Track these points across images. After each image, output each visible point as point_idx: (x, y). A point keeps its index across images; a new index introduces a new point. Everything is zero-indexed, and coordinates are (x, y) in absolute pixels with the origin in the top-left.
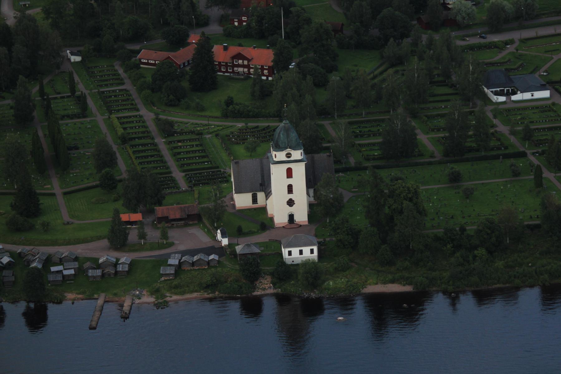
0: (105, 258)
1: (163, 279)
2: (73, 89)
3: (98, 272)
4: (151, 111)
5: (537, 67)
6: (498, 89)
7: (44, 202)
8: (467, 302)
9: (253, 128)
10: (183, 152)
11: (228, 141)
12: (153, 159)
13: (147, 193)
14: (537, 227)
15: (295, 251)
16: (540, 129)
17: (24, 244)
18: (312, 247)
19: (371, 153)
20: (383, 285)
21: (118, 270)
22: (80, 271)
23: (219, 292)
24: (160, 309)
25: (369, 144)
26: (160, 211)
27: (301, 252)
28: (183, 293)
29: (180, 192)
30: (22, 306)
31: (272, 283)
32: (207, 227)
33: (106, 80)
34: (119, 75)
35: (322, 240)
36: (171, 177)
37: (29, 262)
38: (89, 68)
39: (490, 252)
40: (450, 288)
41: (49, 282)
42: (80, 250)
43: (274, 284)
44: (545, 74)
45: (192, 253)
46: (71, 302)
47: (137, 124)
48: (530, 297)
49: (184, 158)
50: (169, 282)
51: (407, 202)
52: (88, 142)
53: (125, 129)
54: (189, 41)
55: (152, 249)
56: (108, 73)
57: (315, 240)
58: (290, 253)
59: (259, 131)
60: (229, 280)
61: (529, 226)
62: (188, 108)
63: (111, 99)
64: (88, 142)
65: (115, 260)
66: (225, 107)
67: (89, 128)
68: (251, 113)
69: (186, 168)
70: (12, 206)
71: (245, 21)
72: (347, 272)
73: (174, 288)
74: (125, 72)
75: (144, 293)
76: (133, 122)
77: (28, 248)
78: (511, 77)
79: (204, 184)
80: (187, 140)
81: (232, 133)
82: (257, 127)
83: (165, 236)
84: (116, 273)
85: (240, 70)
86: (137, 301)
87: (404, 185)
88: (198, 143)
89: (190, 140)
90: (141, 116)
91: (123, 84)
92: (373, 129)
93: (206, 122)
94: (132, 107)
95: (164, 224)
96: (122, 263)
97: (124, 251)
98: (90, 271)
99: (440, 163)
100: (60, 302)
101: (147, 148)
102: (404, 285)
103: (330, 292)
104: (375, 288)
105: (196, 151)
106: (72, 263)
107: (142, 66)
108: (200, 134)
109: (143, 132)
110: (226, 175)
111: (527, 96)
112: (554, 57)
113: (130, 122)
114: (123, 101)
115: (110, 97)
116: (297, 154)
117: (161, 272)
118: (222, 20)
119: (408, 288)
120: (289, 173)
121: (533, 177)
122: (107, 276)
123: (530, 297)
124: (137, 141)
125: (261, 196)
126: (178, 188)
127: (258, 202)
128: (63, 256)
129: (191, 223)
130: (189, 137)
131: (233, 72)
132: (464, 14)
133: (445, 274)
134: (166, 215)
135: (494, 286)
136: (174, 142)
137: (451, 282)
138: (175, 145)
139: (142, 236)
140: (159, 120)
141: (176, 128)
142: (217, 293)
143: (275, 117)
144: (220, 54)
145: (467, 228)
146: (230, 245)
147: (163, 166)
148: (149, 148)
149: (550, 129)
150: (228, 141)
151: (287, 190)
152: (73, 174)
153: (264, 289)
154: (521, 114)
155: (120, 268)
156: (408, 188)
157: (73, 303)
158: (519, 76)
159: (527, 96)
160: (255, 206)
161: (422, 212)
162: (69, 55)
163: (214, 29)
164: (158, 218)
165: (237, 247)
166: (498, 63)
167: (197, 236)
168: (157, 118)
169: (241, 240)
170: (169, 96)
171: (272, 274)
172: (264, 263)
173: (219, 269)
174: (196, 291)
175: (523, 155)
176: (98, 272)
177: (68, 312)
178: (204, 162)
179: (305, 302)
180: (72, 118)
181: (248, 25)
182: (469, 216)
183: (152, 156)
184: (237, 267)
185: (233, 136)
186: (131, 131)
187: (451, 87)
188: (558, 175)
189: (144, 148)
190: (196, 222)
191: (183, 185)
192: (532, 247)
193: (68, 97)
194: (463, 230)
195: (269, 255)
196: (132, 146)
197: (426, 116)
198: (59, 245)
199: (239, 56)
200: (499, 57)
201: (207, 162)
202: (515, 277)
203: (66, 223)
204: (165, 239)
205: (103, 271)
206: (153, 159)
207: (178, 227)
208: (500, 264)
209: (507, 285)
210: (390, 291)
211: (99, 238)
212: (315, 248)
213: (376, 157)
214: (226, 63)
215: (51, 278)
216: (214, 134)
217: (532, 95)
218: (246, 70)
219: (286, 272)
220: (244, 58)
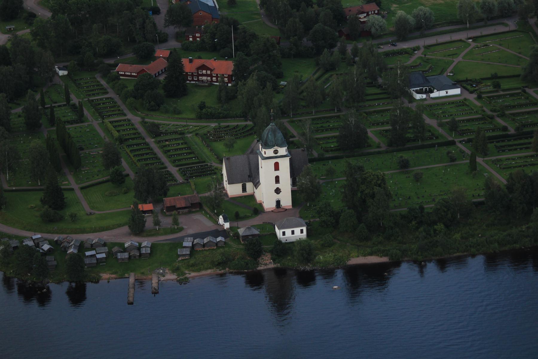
0: (130, 243)
1: (180, 259)
2: (68, 99)
3: (126, 255)
4: (136, 115)
5: (443, 69)
6: (418, 88)
7: (67, 195)
8: (431, 268)
9: (225, 128)
10: (172, 150)
11: (208, 139)
12: (148, 156)
13: (154, 187)
14: (481, 203)
15: (288, 232)
16: (460, 121)
17: (57, 233)
18: (302, 228)
19: (328, 145)
20: (364, 258)
21: (142, 252)
22: (110, 254)
23: (230, 268)
24: (183, 284)
25: (324, 138)
26: (168, 201)
27: (293, 232)
28: (199, 270)
29: (178, 184)
30: (66, 285)
31: (272, 259)
32: (208, 214)
33: (93, 90)
34: (102, 85)
35: (307, 221)
36: (168, 171)
37: (66, 249)
38: (75, 80)
39: (447, 226)
40: (420, 258)
41: (86, 265)
42: (106, 236)
43: (274, 260)
44: (451, 74)
45: (202, 235)
46: (107, 281)
47: (127, 127)
48: (477, 263)
49: (174, 155)
50: (186, 261)
51: (377, 188)
52: (90, 144)
53: (118, 131)
54: (156, 55)
55: (166, 233)
56: (92, 84)
57: (301, 220)
58: (284, 233)
59: (230, 130)
60: (236, 258)
61: (474, 203)
62: (167, 112)
63: (100, 106)
64: (90, 144)
65: (138, 244)
66: (199, 110)
67: (88, 131)
68: (221, 115)
69: (177, 163)
70: (41, 201)
71: (198, 37)
72: (332, 248)
73: (191, 266)
74: (108, 83)
75: (167, 271)
76: (124, 125)
77: (64, 236)
78: (427, 78)
79: (196, 176)
80: (173, 139)
81: (209, 132)
82: (228, 126)
83: (176, 222)
84: (141, 255)
85: (204, 78)
86: (162, 279)
87: (373, 173)
88: (182, 142)
89: (175, 139)
90: (129, 120)
91: (107, 93)
92: (324, 125)
93: (185, 124)
94: (119, 112)
95: (174, 212)
96: (145, 247)
97: (143, 236)
98: (119, 254)
99: (387, 152)
100: (97, 282)
101: (140, 147)
102: (381, 257)
103: (321, 265)
104: (357, 260)
105: (182, 149)
106: (103, 248)
107: (121, 77)
108: (182, 133)
109: (135, 134)
110: (213, 168)
111: (443, 93)
112: (454, 60)
113: (121, 126)
114: (111, 107)
115: (100, 104)
116: (283, 151)
117: (179, 253)
118: (178, 37)
119: (385, 259)
120: (277, 167)
121: (468, 161)
122: (133, 258)
123: (477, 263)
124: (131, 142)
125: (249, 186)
126: (176, 181)
127: (247, 190)
128: (94, 242)
129: (194, 210)
130: (174, 136)
131: (198, 80)
132: (377, 27)
133: (413, 246)
134: (173, 205)
135: (455, 255)
136: (162, 141)
137: (419, 253)
138: (164, 144)
139: (157, 223)
140: (146, 123)
141: (161, 129)
142: (227, 269)
143: (241, 117)
144: (188, 65)
145: (425, 206)
146: (231, 228)
147: (159, 163)
148: (142, 147)
149: (468, 120)
150: (208, 139)
151: (273, 181)
152: (84, 171)
153: (266, 264)
154: (441, 109)
155: (143, 251)
156: (377, 176)
157: (108, 282)
158: (433, 77)
159: (443, 93)
160: (245, 194)
161: (388, 195)
162: (57, 70)
163: (173, 44)
164: (167, 207)
165: (239, 230)
166: (411, 67)
167: (199, 222)
168: (143, 121)
169: (240, 223)
170: (150, 102)
171: (271, 252)
172: (261, 242)
173: (226, 249)
174: (210, 268)
175: (453, 143)
176: (126, 255)
177: (105, 288)
178: (192, 158)
179: (293, 271)
180: (72, 124)
181: (203, 41)
182: (423, 197)
183: (147, 154)
184: (241, 247)
185: (210, 135)
186: (124, 133)
187: (378, 88)
188: (485, 159)
189: (138, 148)
190: (198, 209)
191: (180, 179)
192: (479, 221)
193: (64, 105)
194: (422, 208)
195: (265, 236)
196: (129, 146)
197: (365, 113)
198: (87, 233)
199: (203, 67)
200: (410, 61)
201: (195, 157)
202: (471, 247)
203: (89, 213)
204: (176, 224)
205: (129, 254)
206: (148, 156)
207: (185, 214)
208: (457, 236)
209: (465, 253)
210: (370, 262)
211: (120, 226)
212: (305, 229)
213: (333, 149)
214: (192, 73)
215: (87, 261)
216: (194, 133)
217: (447, 93)
218: (209, 78)
219: (283, 249)
220: (207, 68)
